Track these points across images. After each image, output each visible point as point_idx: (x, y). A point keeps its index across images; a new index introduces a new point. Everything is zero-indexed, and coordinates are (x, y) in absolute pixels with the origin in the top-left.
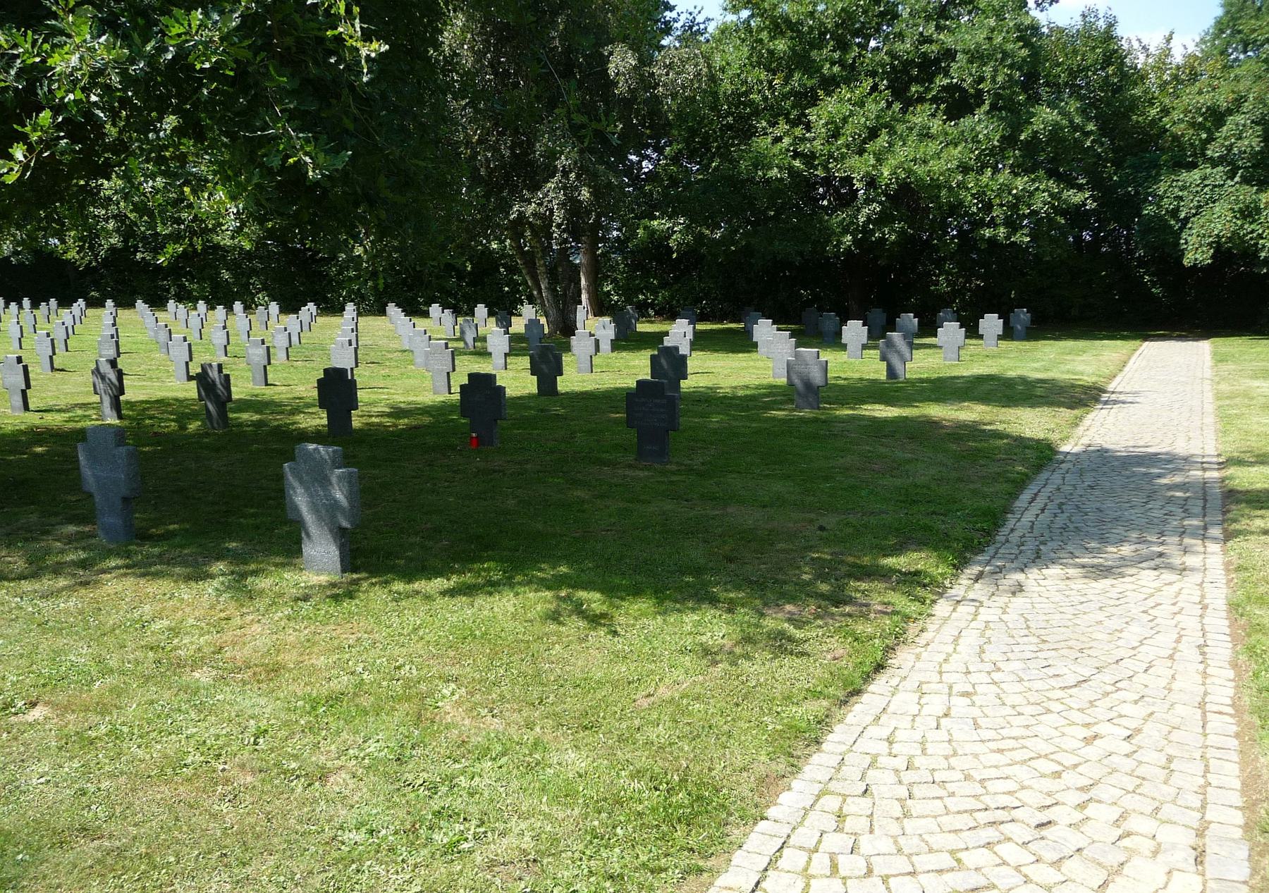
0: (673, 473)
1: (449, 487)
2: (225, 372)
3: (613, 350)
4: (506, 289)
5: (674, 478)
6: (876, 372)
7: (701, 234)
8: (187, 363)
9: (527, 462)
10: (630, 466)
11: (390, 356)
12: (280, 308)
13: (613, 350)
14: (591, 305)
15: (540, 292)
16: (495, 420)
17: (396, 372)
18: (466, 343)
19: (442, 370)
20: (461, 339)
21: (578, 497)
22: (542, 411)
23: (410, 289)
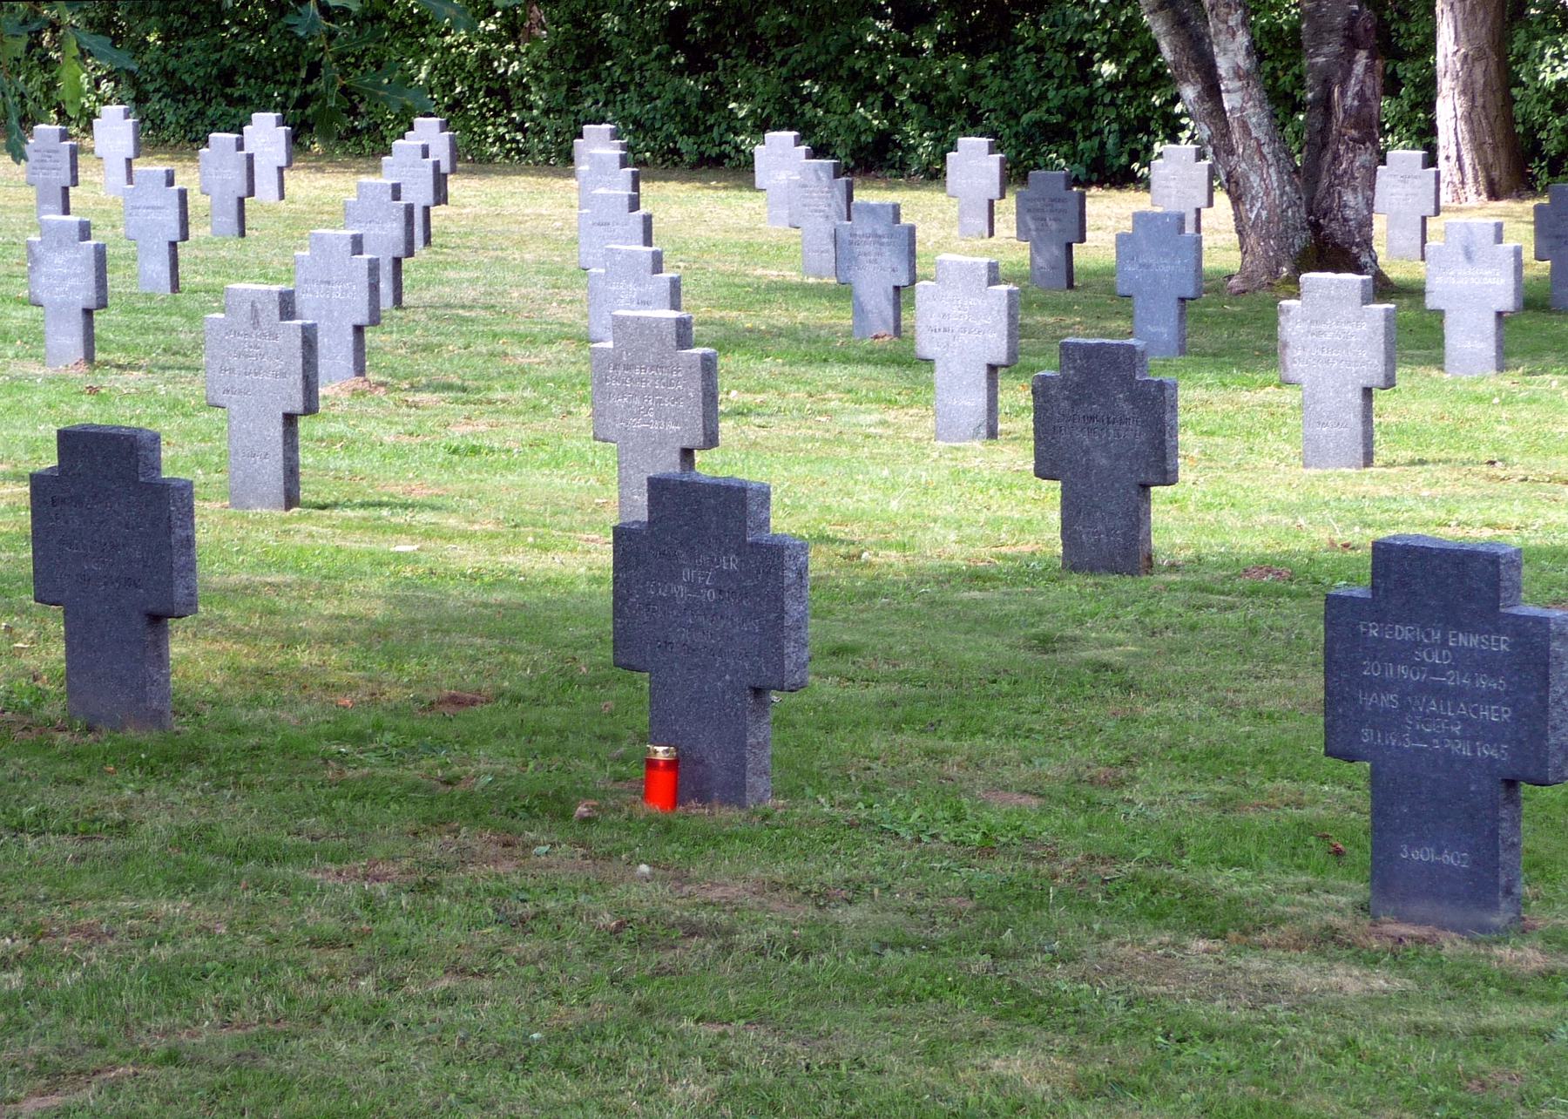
0: (1514, 987)
1: (449, 999)
2: (905, 220)
3: (1504, 358)
4: (1108, 69)
5: (1502, 1014)
6: (1023, 528)
7: (320, 238)
8: (241, 201)
9: (855, 891)
10: (1327, 941)
11: (521, 355)
12: (138, 131)
13: (1504, 358)
14: (1478, 147)
15: (1212, 90)
16: (758, 692)
17: (515, 433)
18: (860, 312)
19: (663, 440)
20: (843, 292)
21: (999, 1083)
22: (1045, 644)
23: (697, 65)
